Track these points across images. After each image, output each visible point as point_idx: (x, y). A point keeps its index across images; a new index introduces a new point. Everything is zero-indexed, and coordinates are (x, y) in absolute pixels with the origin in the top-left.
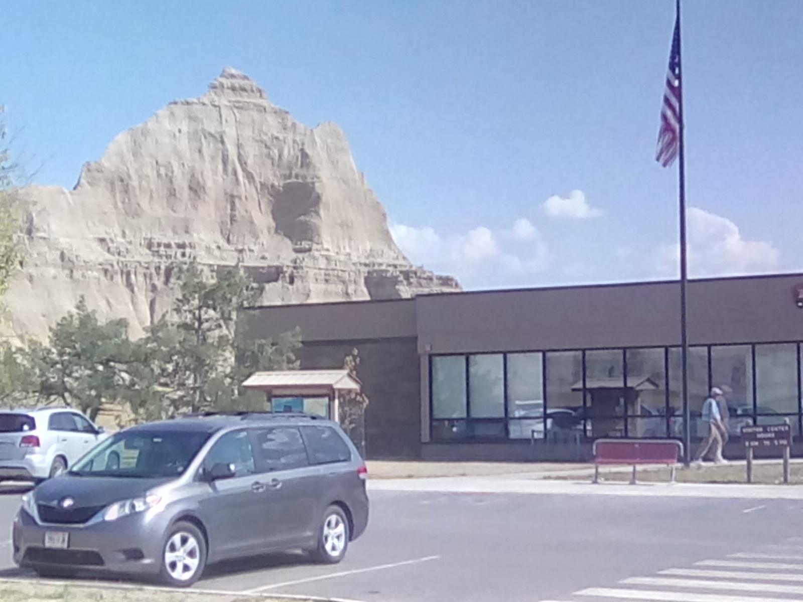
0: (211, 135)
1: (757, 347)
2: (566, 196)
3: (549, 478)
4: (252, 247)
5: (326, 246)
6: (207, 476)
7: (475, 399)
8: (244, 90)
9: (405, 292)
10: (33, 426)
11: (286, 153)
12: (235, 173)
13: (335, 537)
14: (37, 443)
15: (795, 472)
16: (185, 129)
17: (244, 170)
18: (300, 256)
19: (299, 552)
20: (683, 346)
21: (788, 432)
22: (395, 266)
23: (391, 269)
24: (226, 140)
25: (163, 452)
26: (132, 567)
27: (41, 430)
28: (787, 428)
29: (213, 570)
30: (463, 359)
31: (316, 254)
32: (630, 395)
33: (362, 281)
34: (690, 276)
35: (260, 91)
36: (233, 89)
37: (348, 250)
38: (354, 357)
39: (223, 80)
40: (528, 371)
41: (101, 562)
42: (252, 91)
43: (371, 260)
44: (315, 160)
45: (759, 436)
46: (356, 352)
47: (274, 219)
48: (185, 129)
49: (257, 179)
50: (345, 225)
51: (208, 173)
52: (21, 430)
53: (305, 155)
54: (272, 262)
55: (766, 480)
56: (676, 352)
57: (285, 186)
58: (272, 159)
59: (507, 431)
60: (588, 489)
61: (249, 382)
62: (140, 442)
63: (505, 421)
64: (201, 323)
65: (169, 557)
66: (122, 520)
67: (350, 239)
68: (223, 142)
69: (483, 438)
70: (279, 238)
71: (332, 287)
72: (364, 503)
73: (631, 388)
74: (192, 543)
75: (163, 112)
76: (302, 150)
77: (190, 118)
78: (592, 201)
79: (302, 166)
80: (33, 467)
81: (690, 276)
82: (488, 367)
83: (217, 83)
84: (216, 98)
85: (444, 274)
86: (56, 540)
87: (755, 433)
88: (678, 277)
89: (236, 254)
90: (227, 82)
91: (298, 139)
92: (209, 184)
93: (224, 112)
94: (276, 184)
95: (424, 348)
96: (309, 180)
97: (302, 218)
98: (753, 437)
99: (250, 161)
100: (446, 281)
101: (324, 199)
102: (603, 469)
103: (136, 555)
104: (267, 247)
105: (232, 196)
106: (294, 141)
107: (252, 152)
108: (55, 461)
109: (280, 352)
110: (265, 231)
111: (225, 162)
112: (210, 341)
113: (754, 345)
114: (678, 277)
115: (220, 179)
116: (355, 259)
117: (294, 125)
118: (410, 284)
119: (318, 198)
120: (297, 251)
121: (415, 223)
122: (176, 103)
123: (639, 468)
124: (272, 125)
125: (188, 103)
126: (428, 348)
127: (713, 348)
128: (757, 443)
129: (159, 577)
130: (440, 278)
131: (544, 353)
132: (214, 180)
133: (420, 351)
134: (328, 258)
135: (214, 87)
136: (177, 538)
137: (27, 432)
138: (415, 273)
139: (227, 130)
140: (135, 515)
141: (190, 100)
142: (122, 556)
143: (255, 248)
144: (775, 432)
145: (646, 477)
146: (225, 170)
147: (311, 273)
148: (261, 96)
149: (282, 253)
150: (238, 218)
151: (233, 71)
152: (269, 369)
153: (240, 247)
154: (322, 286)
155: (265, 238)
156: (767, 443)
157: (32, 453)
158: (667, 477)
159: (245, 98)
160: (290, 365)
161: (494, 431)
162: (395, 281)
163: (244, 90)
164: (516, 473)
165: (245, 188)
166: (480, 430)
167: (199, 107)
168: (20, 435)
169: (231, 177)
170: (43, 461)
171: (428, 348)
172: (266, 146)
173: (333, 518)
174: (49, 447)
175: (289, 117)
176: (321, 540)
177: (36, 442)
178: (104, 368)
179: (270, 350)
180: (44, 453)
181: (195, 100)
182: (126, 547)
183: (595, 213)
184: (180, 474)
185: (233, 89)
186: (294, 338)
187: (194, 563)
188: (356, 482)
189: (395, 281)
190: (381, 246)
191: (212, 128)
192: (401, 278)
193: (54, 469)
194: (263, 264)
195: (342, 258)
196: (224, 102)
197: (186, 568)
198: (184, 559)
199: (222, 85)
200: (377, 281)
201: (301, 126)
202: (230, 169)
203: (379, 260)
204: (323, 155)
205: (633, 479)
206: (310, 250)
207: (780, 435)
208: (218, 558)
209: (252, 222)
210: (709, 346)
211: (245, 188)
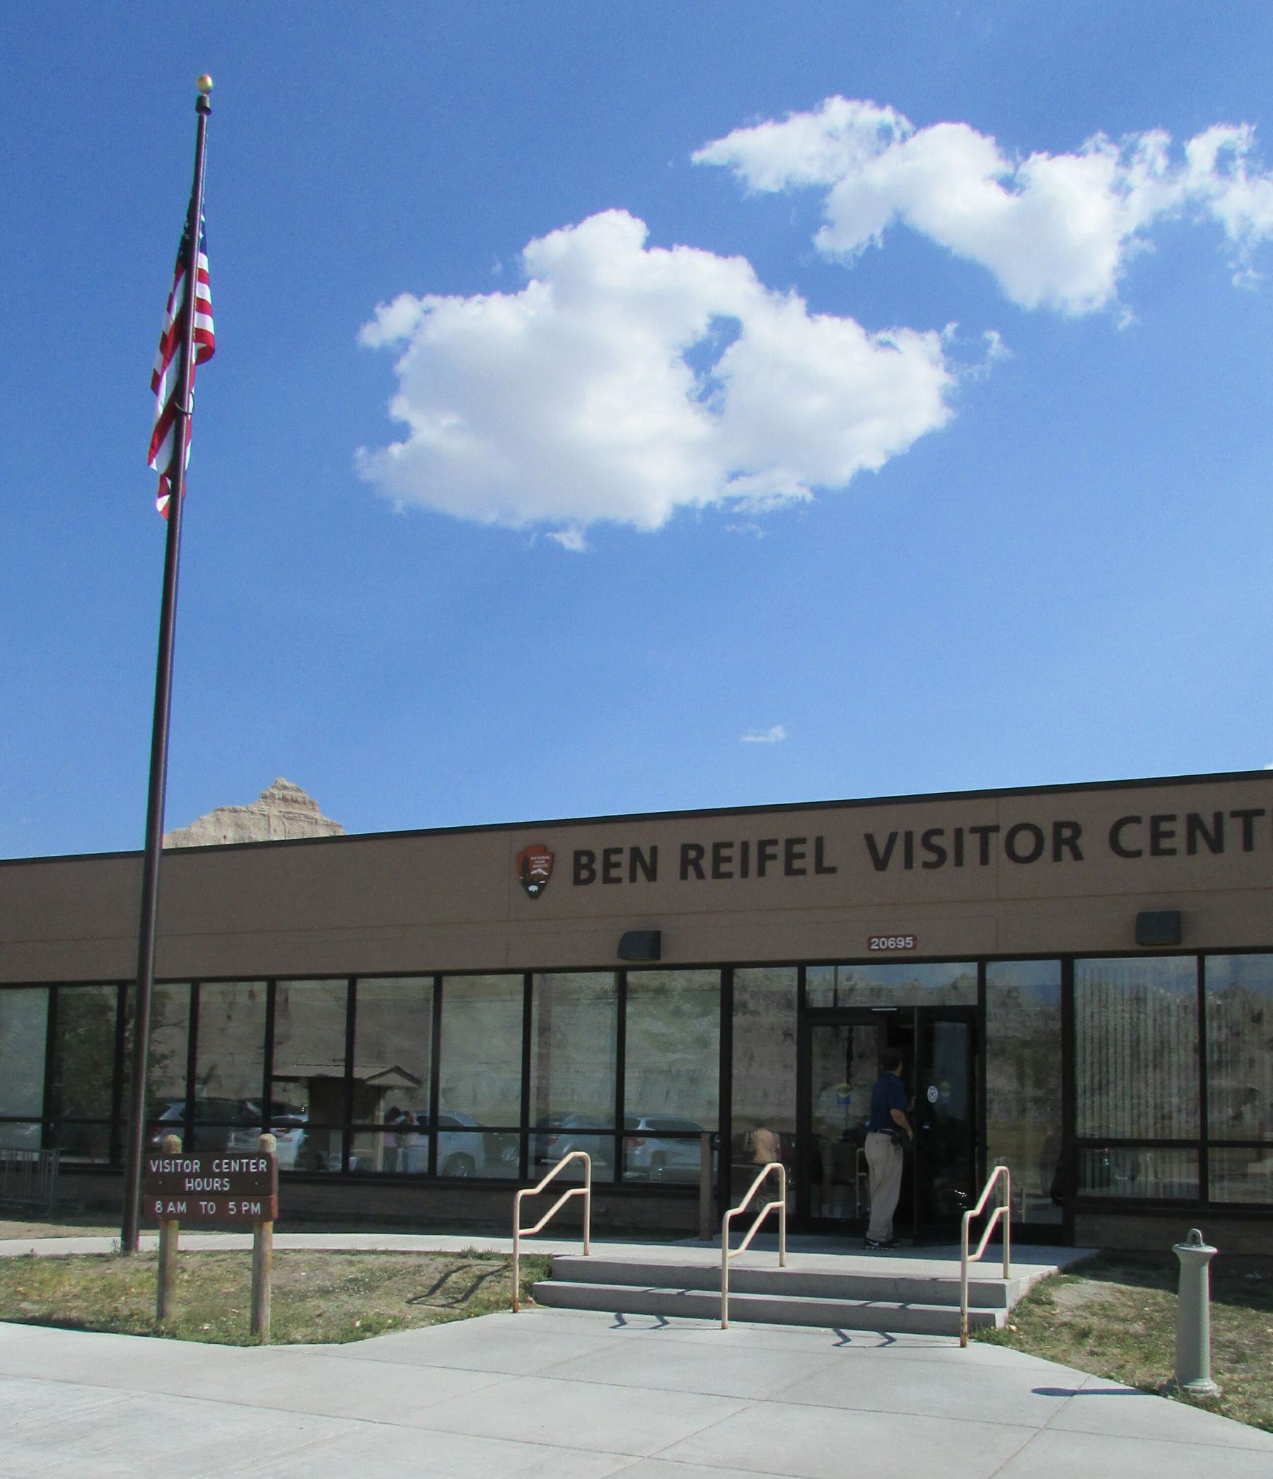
1: (449, 984)
8: (295, 801)
28: (263, 1165)
36: (284, 799)
39: (275, 791)
42: (304, 803)
45: (189, 1185)
73: (361, 1081)
75: (208, 818)
83: (268, 793)
87: (182, 1176)
93: (274, 822)
122: (222, 810)
127: (361, 985)
128: (182, 1208)
135: (265, 797)
141: (238, 808)
144: (232, 1176)
151: (286, 784)
159: (296, 809)
163: (295, 801)
164: (633, 1206)
167: (246, 815)
185: (284, 799)
196: (274, 811)
199: (273, 795)
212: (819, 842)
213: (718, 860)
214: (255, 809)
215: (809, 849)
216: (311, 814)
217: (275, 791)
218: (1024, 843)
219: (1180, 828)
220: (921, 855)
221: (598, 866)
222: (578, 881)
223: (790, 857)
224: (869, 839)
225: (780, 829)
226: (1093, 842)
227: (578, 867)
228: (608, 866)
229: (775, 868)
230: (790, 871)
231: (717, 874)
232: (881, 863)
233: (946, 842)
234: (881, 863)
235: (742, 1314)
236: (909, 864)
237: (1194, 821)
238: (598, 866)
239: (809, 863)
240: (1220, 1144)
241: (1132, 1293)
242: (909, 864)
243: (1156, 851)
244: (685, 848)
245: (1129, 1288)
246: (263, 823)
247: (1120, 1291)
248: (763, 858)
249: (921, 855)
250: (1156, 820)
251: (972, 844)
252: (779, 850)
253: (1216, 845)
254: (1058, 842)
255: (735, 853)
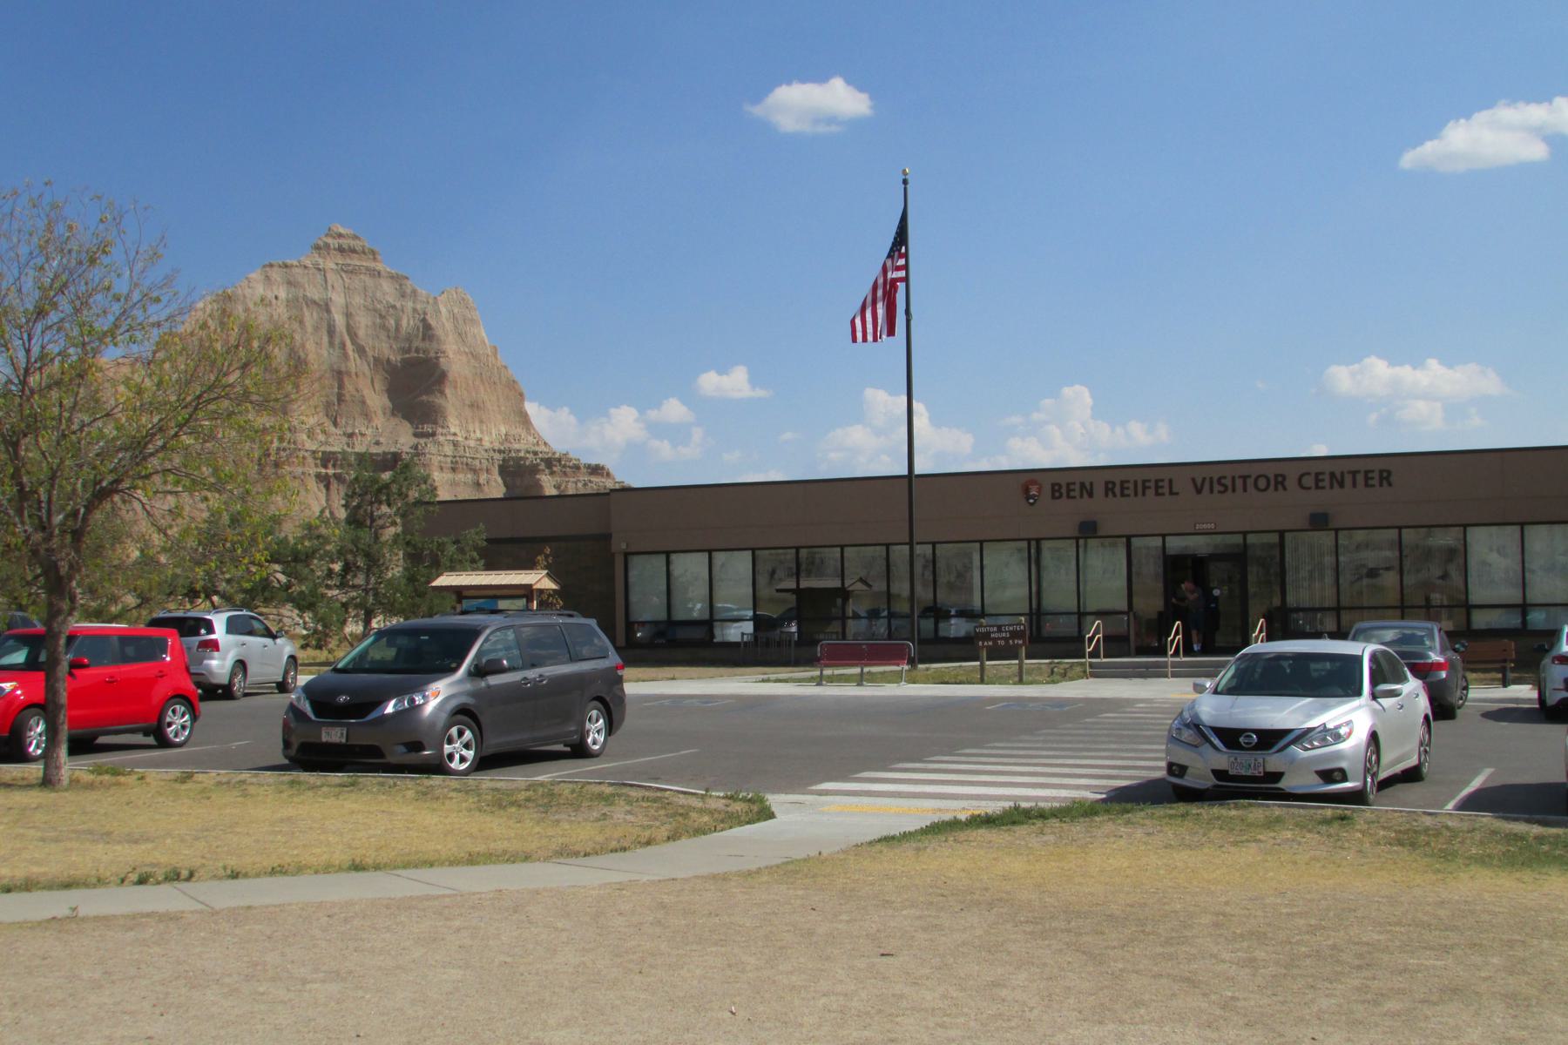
0: (315, 302)
2: (723, 371)
3: (768, 681)
4: (363, 430)
5: (453, 430)
6: (479, 672)
7: (676, 601)
8: (354, 251)
9: (549, 485)
10: (211, 630)
11: (404, 323)
12: (343, 346)
13: (595, 734)
14: (217, 649)
15: (1029, 673)
16: (282, 294)
17: (354, 342)
18: (422, 441)
19: (560, 747)
20: (911, 544)
21: (1023, 632)
22: (535, 453)
23: (530, 456)
24: (333, 309)
25: (431, 652)
26: (412, 758)
27: (220, 633)
29: (485, 763)
30: (663, 557)
31: (441, 439)
32: (844, 594)
33: (496, 471)
34: (918, 470)
35: (373, 253)
36: (341, 250)
37: (478, 435)
38: (547, 557)
39: (330, 241)
40: (737, 567)
41: (382, 755)
43: (507, 445)
44: (439, 332)
46: (548, 551)
47: (391, 399)
48: (282, 294)
49: (370, 353)
50: (475, 406)
51: (310, 346)
52: (198, 634)
53: (427, 327)
54: (387, 447)
55: (1001, 680)
56: (900, 552)
57: (403, 360)
58: (388, 331)
59: (712, 636)
60: (811, 690)
61: (437, 583)
62: (403, 641)
63: (708, 624)
64: (373, 520)
65: (447, 748)
66: (397, 714)
67: (481, 422)
68: (328, 311)
69: (685, 642)
70: (394, 421)
71: (460, 477)
72: (621, 698)
74: (468, 735)
76: (424, 320)
77: (289, 283)
78: (754, 381)
79: (423, 339)
80: (211, 673)
81: (918, 470)
82: (690, 567)
84: (321, 261)
85: (594, 462)
86: (334, 735)
88: (905, 472)
89: (345, 439)
90: (333, 243)
91: (419, 307)
92: (311, 357)
94: (392, 358)
95: (619, 545)
96: (432, 355)
97: (424, 398)
98: (986, 636)
99: (361, 333)
100: (596, 470)
101: (451, 376)
102: (828, 672)
103: (417, 746)
104: (383, 432)
105: (340, 373)
106: (415, 310)
107: (363, 322)
108: (234, 667)
109: (461, 551)
110: (380, 412)
111: (331, 331)
112: (383, 539)
113: (981, 542)
114: (905, 472)
115: (325, 353)
116: (487, 445)
117: (414, 292)
118: (552, 473)
119: (443, 376)
120: (416, 435)
121: (552, 406)
122: (271, 266)
123: (866, 669)
124: (388, 291)
125: (286, 266)
126: (624, 546)
129: (438, 767)
130: (589, 467)
131: (753, 550)
132: (318, 353)
133: (614, 549)
134: (455, 444)
135: (317, 248)
136: (454, 731)
137: (204, 636)
138: (559, 460)
139: (334, 297)
140: (415, 708)
141: (289, 262)
142: (402, 749)
143: (369, 432)
145: (873, 679)
146: (331, 344)
147: (436, 460)
148: (375, 259)
149: (401, 438)
150: (348, 397)
151: (342, 231)
152: (452, 569)
153: (350, 431)
154: (448, 476)
155: (379, 421)
156: (1002, 643)
157: (212, 658)
158: (896, 678)
159: (355, 261)
160: (473, 566)
161: (698, 634)
162: (534, 470)
163: (354, 251)
165: (355, 363)
166: (682, 634)
168: (196, 640)
169: (337, 352)
170: (222, 667)
171: (624, 546)
172: (381, 316)
173: (594, 713)
174: (228, 651)
175: (409, 283)
176: (584, 734)
177: (214, 645)
178: (136, 563)
179: (452, 549)
180: (223, 659)
181: (295, 263)
182: (408, 740)
183: (760, 393)
184: (455, 670)
185: (341, 250)
186: (476, 535)
187: (470, 754)
188: (614, 680)
189: (534, 470)
190: (519, 430)
191: (314, 293)
192: (542, 466)
193: (233, 674)
194: (375, 450)
195: (472, 443)
197: (463, 759)
198: (460, 752)
199: (327, 246)
200: (516, 470)
201: (422, 292)
202: (337, 341)
203: (517, 446)
204: (449, 326)
205: (860, 680)
206: (433, 434)
207: (1014, 635)
208: (490, 751)
209: (364, 402)
210: (934, 544)
211: (355, 363)
212: (1171, 481)
213: (1122, 488)
214: (308, 263)
215: (1166, 484)
216: (372, 265)
217: (330, 241)
218: (1262, 483)
219: (1327, 477)
220: (1217, 488)
221: (1064, 490)
222: (1053, 497)
223: (1157, 487)
224: (1194, 480)
225: (1152, 475)
226: (1291, 483)
227: (1053, 491)
228: (1069, 491)
229: (1150, 492)
230: (1157, 494)
231: (1123, 495)
232: (1199, 491)
233: (1228, 482)
234: (1199, 491)
235: (1175, 675)
236: (1212, 491)
237: (1332, 475)
238: (1064, 490)
239: (1166, 490)
240: (1329, 609)
241: (1540, 839)
242: (1212, 491)
243: (1317, 487)
244: (1107, 483)
245: (1536, 830)
246: (319, 278)
247: (1518, 837)
248: (1145, 488)
249: (1217, 488)
250: (1317, 474)
251: (1239, 483)
252: (1152, 484)
253: (1341, 485)
254: (1277, 483)
255: (1131, 486)
